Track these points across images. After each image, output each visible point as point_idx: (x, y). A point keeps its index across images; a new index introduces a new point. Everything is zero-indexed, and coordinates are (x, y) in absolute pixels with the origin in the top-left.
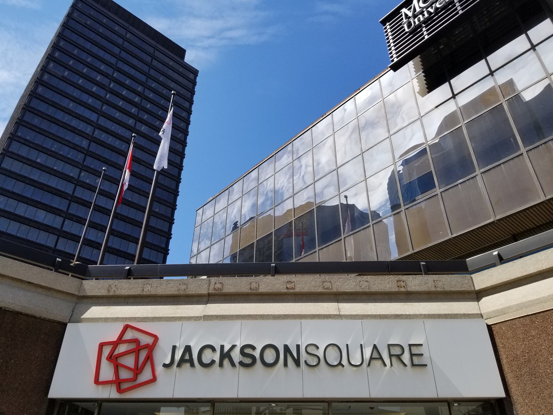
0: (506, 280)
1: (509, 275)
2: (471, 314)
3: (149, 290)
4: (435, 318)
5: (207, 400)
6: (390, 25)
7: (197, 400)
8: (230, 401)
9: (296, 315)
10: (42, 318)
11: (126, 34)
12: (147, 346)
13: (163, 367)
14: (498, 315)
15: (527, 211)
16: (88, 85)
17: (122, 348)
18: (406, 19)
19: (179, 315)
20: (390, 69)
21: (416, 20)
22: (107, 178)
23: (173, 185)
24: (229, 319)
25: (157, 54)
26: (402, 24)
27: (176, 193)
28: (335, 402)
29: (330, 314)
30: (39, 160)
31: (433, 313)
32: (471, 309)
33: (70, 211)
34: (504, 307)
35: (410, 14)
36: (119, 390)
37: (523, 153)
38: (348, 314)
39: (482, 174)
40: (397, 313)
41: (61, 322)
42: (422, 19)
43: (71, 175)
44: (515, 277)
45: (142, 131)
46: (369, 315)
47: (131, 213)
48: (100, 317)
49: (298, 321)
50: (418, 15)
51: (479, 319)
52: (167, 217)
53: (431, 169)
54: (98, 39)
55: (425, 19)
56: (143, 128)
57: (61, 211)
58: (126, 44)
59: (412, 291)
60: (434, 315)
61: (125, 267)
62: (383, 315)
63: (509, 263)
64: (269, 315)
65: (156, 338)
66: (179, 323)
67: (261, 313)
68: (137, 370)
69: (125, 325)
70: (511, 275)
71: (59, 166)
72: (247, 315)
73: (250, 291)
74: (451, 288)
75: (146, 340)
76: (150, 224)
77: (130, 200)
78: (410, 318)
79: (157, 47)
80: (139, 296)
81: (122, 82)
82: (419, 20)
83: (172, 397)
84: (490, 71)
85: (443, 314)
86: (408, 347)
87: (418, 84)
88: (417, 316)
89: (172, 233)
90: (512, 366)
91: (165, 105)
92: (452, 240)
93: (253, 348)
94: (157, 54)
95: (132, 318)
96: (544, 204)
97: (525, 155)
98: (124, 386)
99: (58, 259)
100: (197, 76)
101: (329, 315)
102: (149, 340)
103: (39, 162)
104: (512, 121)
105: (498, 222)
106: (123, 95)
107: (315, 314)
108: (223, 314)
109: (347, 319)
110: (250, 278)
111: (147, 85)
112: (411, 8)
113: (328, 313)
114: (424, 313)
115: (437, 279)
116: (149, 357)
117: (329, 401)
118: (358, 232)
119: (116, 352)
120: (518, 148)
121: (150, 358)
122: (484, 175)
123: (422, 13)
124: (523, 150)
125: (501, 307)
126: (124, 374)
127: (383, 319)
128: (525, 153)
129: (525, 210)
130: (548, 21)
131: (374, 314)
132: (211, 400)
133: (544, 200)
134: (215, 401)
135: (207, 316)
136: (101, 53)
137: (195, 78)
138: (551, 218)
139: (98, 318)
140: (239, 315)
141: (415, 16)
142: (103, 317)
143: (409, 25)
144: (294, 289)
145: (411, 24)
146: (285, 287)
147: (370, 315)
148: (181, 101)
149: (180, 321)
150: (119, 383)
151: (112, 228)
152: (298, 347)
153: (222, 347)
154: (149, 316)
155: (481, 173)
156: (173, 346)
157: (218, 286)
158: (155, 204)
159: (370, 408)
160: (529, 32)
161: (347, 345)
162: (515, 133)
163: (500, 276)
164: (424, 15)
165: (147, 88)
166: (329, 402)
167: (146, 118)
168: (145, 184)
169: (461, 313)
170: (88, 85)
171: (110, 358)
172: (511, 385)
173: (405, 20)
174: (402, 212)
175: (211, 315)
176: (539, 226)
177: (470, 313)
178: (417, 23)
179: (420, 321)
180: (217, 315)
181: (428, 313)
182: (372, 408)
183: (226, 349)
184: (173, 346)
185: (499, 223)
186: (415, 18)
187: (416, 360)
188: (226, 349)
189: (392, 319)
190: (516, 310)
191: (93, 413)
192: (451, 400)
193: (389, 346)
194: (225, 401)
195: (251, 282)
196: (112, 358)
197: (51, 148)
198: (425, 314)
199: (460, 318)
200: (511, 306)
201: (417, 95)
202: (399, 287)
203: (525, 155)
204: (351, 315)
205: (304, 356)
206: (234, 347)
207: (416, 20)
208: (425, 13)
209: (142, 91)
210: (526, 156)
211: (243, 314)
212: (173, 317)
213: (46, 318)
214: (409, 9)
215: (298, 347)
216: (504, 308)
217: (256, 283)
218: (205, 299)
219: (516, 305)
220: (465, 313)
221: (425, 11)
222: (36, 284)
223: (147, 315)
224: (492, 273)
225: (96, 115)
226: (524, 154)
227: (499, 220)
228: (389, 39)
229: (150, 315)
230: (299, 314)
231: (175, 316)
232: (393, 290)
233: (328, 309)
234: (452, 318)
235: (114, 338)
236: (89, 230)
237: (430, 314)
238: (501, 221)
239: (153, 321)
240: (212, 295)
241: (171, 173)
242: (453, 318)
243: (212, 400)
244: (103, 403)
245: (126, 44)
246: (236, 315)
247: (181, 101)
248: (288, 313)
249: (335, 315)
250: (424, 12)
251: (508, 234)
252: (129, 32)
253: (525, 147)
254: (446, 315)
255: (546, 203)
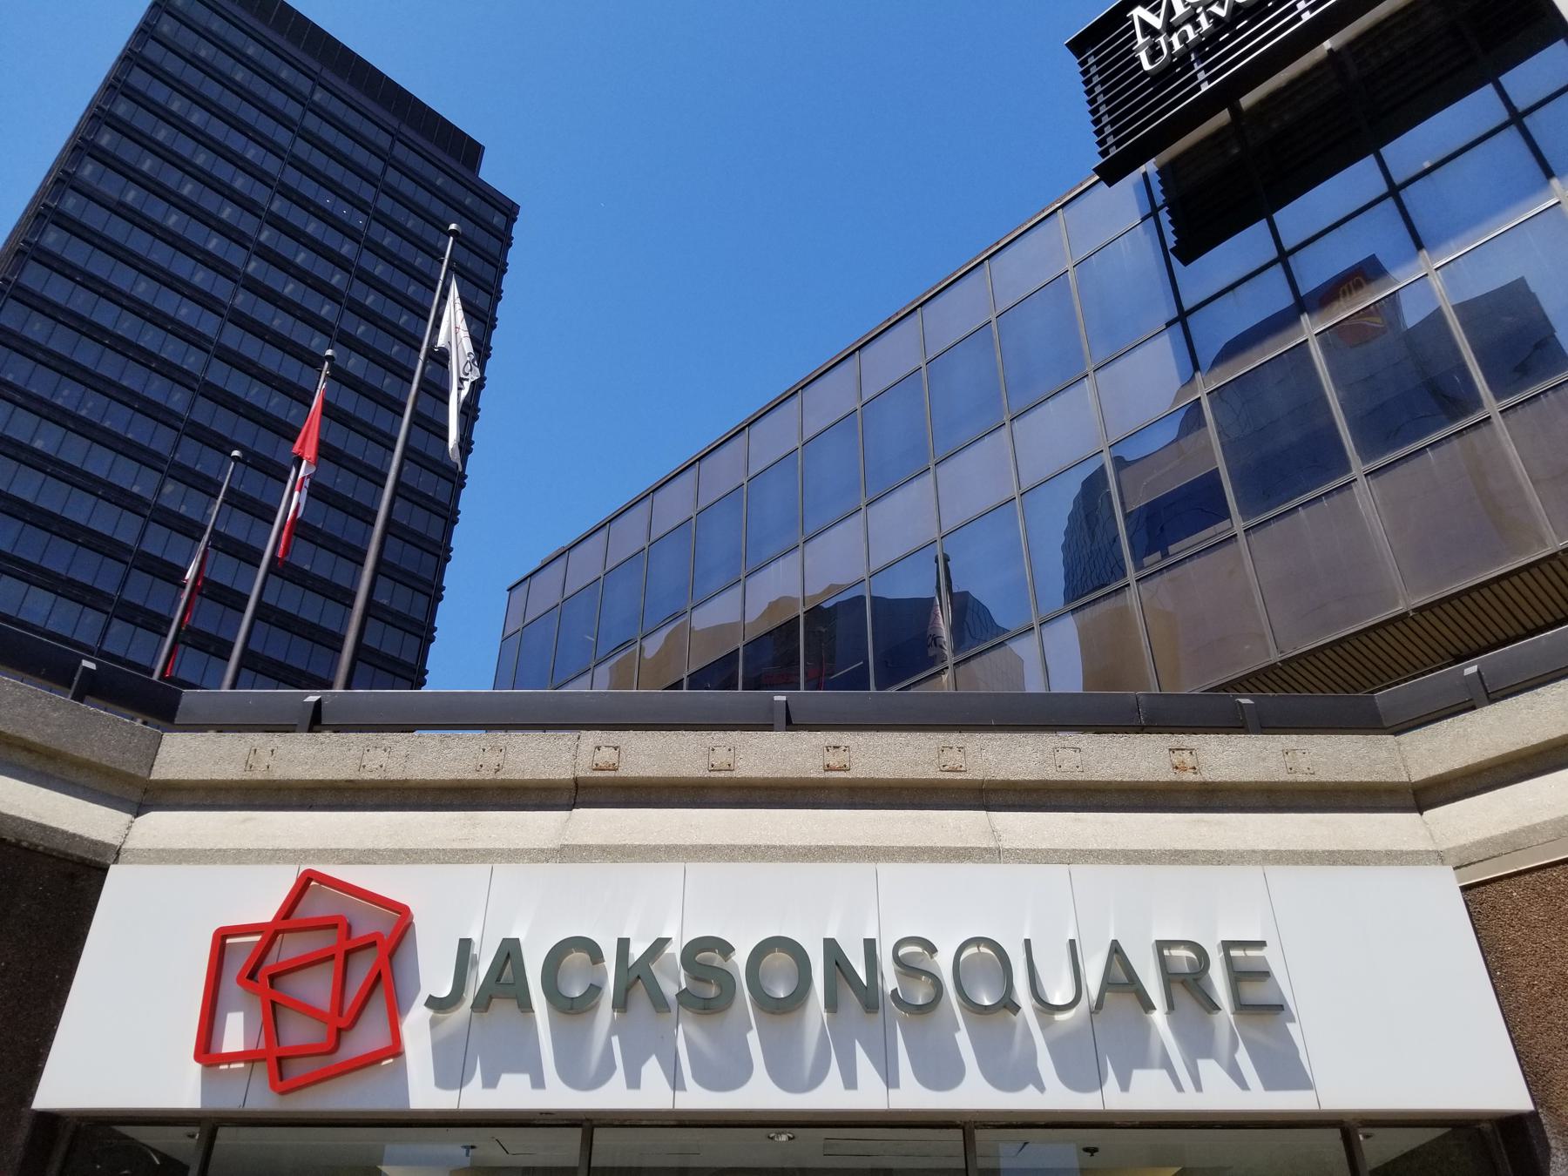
0: (1514, 749)
1: (1524, 734)
2: (1407, 853)
3: (381, 766)
4: (1297, 864)
5: (570, 1120)
6: (1095, 54)
7: (541, 1117)
8: (644, 1123)
9: (862, 847)
10: (25, 844)
11: (313, 92)
12: (370, 943)
13: (425, 1007)
14: (1496, 854)
15: (1495, 587)
16: (195, 232)
17: (290, 948)
18: (1144, 36)
19: (479, 845)
20: (1097, 177)
21: (1175, 39)
22: (253, 460)
23: (434, 529)
24: (644, 859)
25: (400, 151)
26: (1134, 51)
27: (442, 553)
28: (985, 1126)
29: (969, 845)
30: (38, 444)
31: (1291, 849)
32: (1405, 839)
33: (129, 596)
34: (1515, 827)
35: (1157, 22)
36: (282, 1082)
37: (1489, 417)
38: (1024, 848)
39: (1369, 477)
40: (1180, 846)
41: (88, 862)
42: (1192, 35)
43: (136, 489)
44: (1543, 740)
45: (358, 337)
46: (1091, 851)
47: (311, 608)
48: (219, 846)
49: (866, 868)
50: (1180, 27)
51: (1433, 866)
52: (413, 621)
53: (1216, 464)
54: (230, 102)
55: (1201, 36)
56: (352, 362)
57: (100, 594)
58: (312, 122)
59: (1220, 782)
60: (1294, 853)
61: (307, 697)
62: (1135, 851)
63: (1520, 697)
64: (775, 847)
65: (403, 912)
66: (480, 870)
67: (748, 842)
68: (342, 1022)
69: (301, 872)
70: (1528, 734)
71: (100, 463)
72: (703, 846)
73: (707, 774)
74: (1338, 774)
75: (367, 923)
76: (366, 641)
77: (307, 567)
78: (1219, 863)
79: (403, 134)
80: (351, 785)
81: (294, 227)
82: (1183, 38)
83: (455, 1107)
84: (1389, 187)
85: (1324, 852)
86: (1222, 954)
87: (1173, 229)
88: (1242, 857)
89: (427, 668)
90: (1550, 1012)
91: (418, 299)
92: (1281, 668)
93: (726, 949)
94: (400, 151)
95: (326, 850)
96: (1556, 564)
97: (1498, 420)
98: (297, 1069)
99: (85, 663)
100: (515, 220)
101: (966, 849)
102: (381, 923)
103: (39, 448)
104: (1457, 329)
105: (1419, 616)
106: (297, 267)
107: (922, 844)
108: (624, 843)
109: (1023, 863)
110: (708, 734)
111: (394, 157)
112: (1159, 6)
113: (960, 845)
114: (1264, 847)
115: (1293, 745)
116: (379, 976)
117: (965, 1123)
118: (981, 653)
119: (271, 960)
120: (1478, 403)
121: (383, 978)
122: (1374, 481)
123: (1192, 19)
124: (1491, 405)
125: (1505, 829)
126: (299, 1032)
127: (1134, 864)
128: (1496, 415)
129: (1498, 579)
130: (1561, 42)
131: (1108, 848)
132: (582, 1120)
133: (1555, 551)
134: (595, 1122)
135: (573, 847)
136: (236, 142)
137: (509, 227)
138: (1562, 611)
139: (211, 849)
140: (675, 847)
141: (1170, 28)
142: (231, 846)
143: (1154, 53)
144: (844, 769)
145: (1161, 49)
146: (819, 762)
147: (1095, 851)
148: (474, 263)
149: (483, 862)
150: (280, 1060)
151: (263, 599)
152: (870, 945)
153: (623, 944)
154: (382, 846)
155: (1366, 475)
156: (461, 940)
157: (607, 756)
158: (383, 582)
159: (1086, 1150)
160: (1504, 79)
161: (1027, 942)
162: (1466, 358)
163: (1491, 737)
164: (1197, 26)
165: (386, 193)
166: (966, 1128)
167: (363, 334)
168: (356, 525)
169: (1376, 848)
170: (195, 232)
171: (252, 976)
172: (1548, 1072)
173: (1140, 40)
174: (1129, 589)
175: (586, 846)
176: (1543, 626)
177: (1405, 848)
178: (1177, 46)
179: (1253, 872)
180: (607, 846)
181: (1275, 848)
182: (1092, 1151)
183: (637, 951)
184: (461, 940)
185: (1419, 618)
186: (1170, 35)
187: (1253, 993)
188: (637, 951)
189: (1164, 863)
190: (1553, 838)
191: (186, 1168)
192: (1354, 1119)
193: (1161, 945)
194: (627, 1123)
195: (712, 746)
196: (258, 976)
197: (77, 409)
198: (1265, 851)
199: (1376, 864)
200: (1538, 824)
201: (1173, 259)
202: (1177, 768)
203: (1498, 420)
204: (1034, 850)
205: (890, 980)
206: (661, 943)
207: (1175, 39)
208: (1202, 19)
209: (352, 257)
210: (1152, 673)
211: (688, 843)
212: (461, 850)
213: (37, 846)
214: (1155, 10)
215: (870, 945)
216: (1515, 832)
217: (730, 750)
218: (565, 797)
219: (1551, 822)
220: (1390, 848)
221: (1201, 12)
222: (10, 735)
223: (376, 842)
224: (1465, 730)
225: (216, 319)
226: (1494, 420)
227: (1419, 610)
228: (1094, 92)
229: (384, 844)
230: (870, 844)
231: (467, 848)
232: (1162, 779)
233: (960, 831)
234: (1350, 864)
235: (266, 912)
236: (184, 652)
237: (1280, 851)
238: (1427, 614)
239: (393, 862)
240: (585, 787)
241: (430, 494)
242: (1355, 864)
243: (588, 1120)
244: (220, 1129)
245: (312, 122)
246: (667, 846)
247: (474, 263)
248: (833, 843)
249: (985, 849)
250: (1198, 15)
251: (1441, 651)
252: (321, 85)
253: (1498, 398)
254: (1331, 853)
255: (1559, 559)
